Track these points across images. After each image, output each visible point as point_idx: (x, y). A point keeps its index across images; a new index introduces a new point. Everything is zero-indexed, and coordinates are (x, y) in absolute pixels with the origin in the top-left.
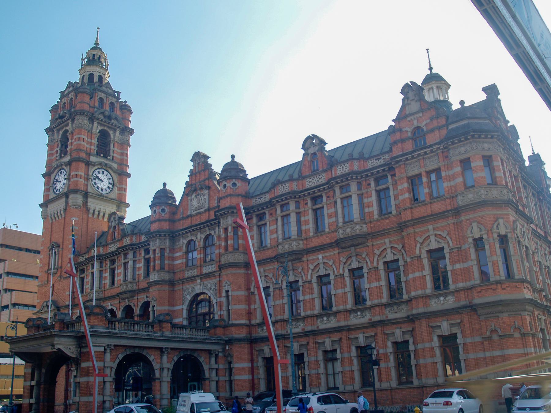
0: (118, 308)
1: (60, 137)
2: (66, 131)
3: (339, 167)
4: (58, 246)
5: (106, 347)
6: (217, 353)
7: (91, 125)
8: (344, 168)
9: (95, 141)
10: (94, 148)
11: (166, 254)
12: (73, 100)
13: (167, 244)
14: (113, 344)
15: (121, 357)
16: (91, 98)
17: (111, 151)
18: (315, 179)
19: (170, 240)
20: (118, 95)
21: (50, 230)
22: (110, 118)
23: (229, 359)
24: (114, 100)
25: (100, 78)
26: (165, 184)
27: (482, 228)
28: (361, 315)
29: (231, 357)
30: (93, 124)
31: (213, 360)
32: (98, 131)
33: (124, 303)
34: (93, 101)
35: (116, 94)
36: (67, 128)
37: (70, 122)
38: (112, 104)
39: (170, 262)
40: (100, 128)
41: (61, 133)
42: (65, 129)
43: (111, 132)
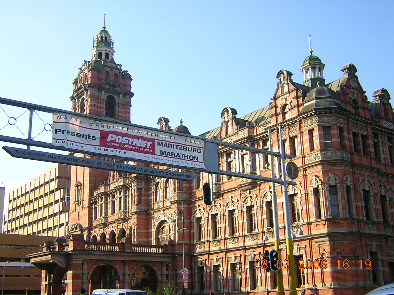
0: (127, 227)
1: (80, 104)
2: (83, 99)
3: (241, 132)
4: (81, 185)
5: (84, 261)
6: (167, 263)
7: (100, 94)
8: (244, 133)
9: (103, 105)
10: (103, 110)
11: (142, 193)
12: (87, 75)
13: (143, 185)
14: (88, 259)
15: (95, 267)
16: (99, 73)
17: (117, 111)
18: (229, 140)
19: (145, 182)
20: (121, 67)
21: (76, 172)
22: (114, 86)
23: (175, 267)
24: (117, 72)
25: (107, 55)
26: (181, 122)
27: (337, 178)
28: (252, 239)
29: (177, 266)
30: (101, 93)
31: (164, 268)
32: (105, 98)
33: (120, 226)
34: (101, 75)
35: (119, 67)
36: (84, 96)
37: (85, 92)
38: (116, 74)
39: (146, 198)
40: (107, 95)
41: (80, 100)
42: (82, 97)
43: (116, 97)
